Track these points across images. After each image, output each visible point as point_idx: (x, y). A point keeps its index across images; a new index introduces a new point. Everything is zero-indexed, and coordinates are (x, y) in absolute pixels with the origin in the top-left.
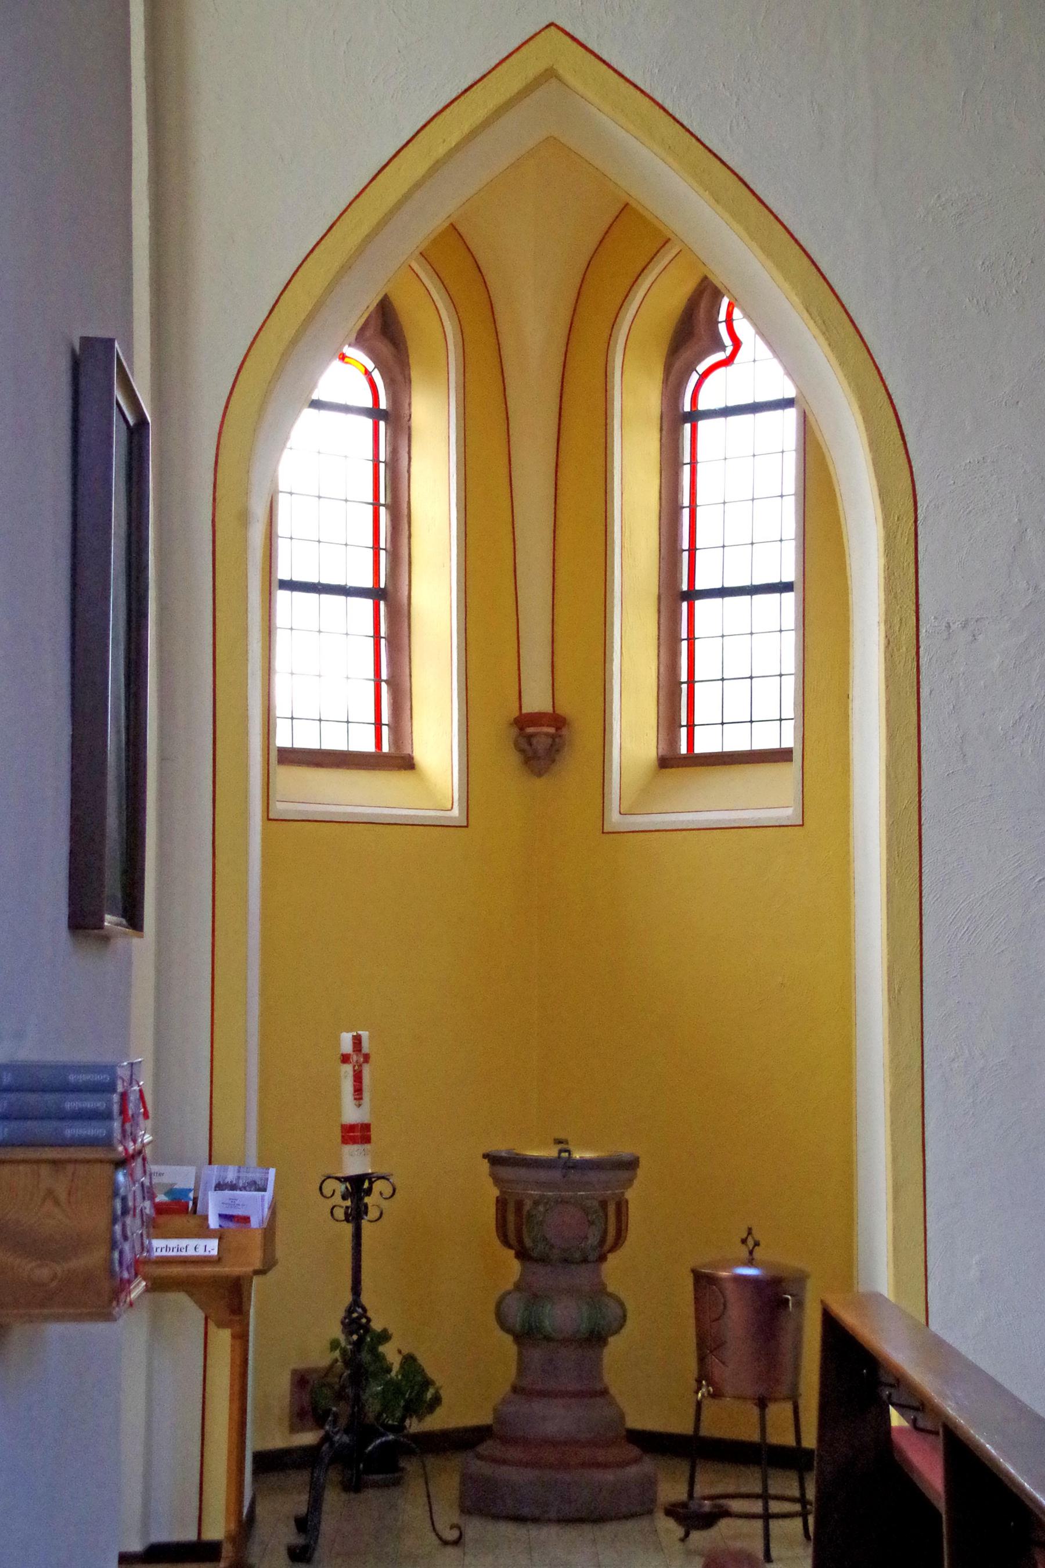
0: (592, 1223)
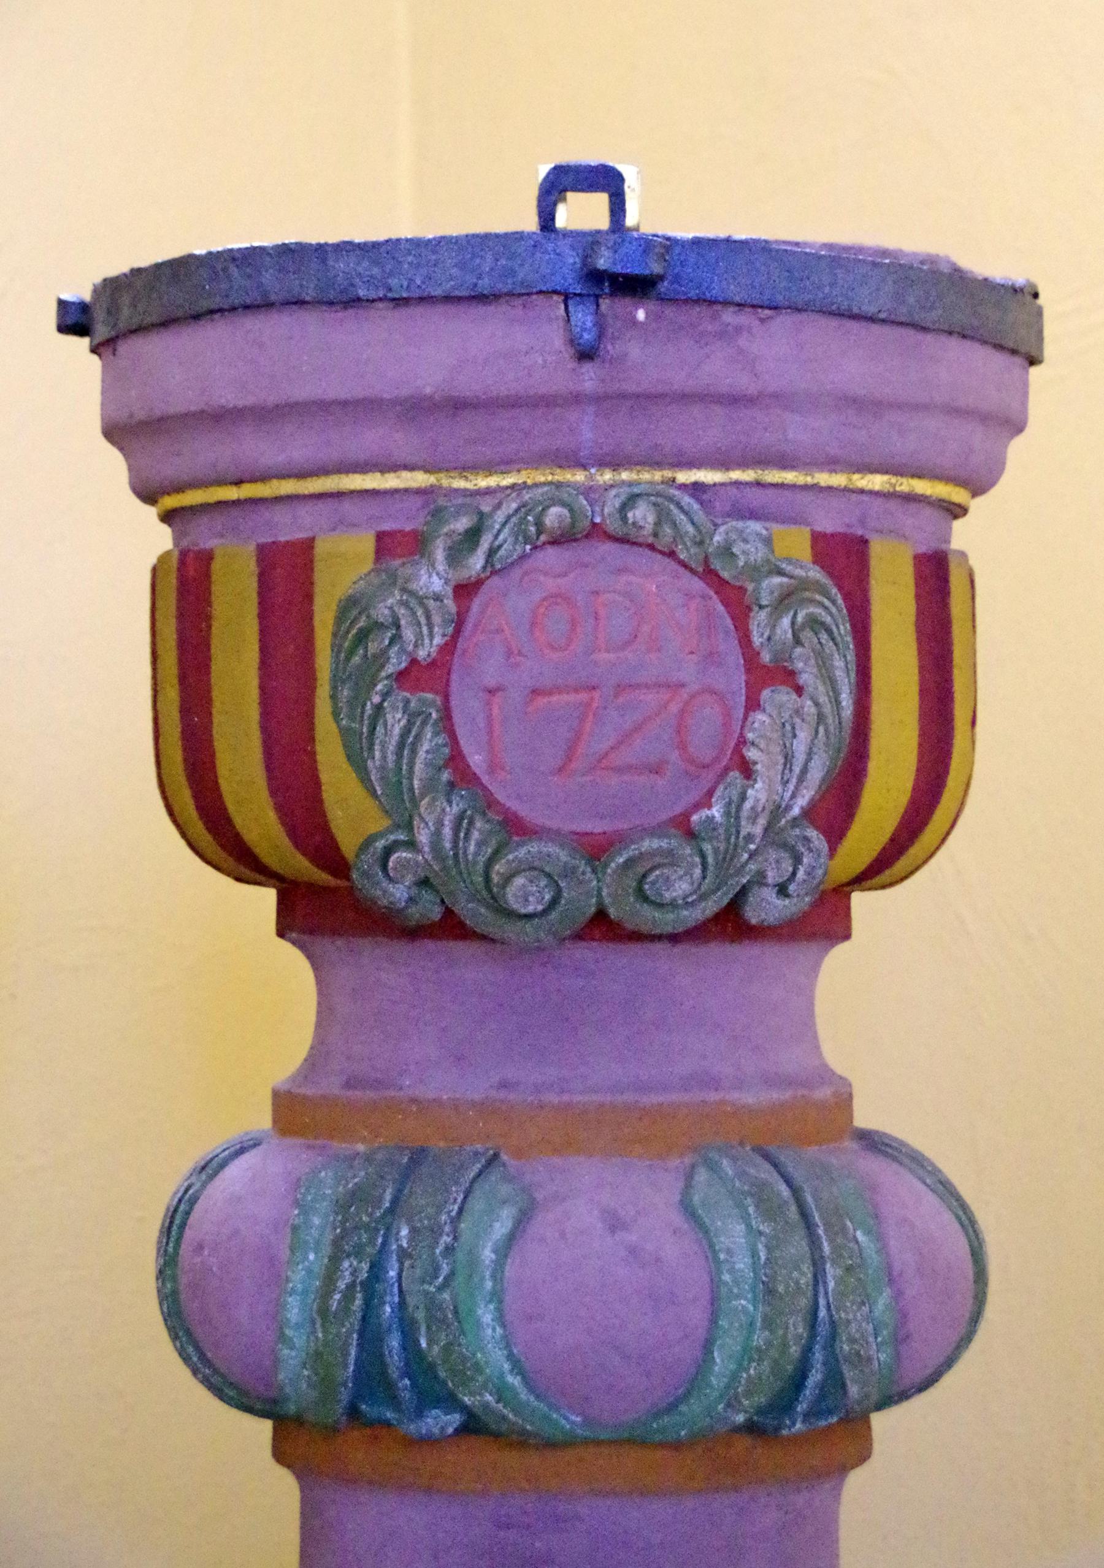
0: (767, 674)
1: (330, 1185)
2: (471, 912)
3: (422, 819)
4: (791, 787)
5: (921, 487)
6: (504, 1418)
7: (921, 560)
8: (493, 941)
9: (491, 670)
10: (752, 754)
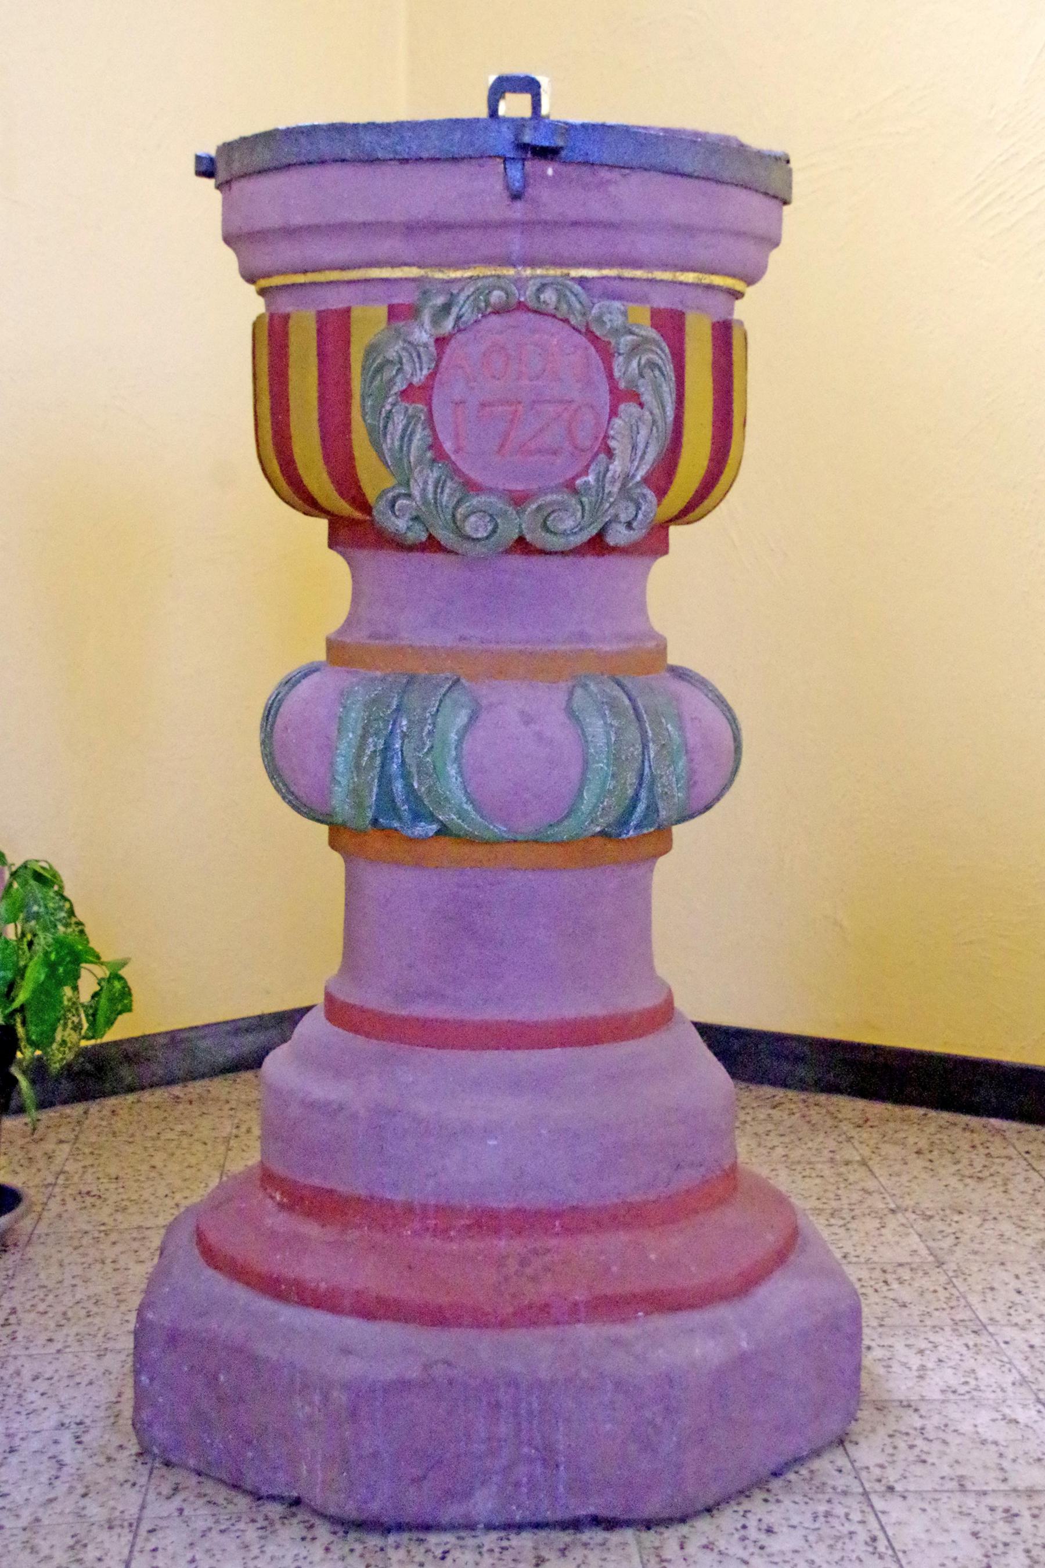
0: (621, 395)
1: (361, 695)
2: (444, 536)
3: (416, 481)
4: (636, 463)
5: (718, 280)
6: (461, 828)
7: (715, 326)
8: (457, 554)
9: (458, 391)
10: (612, 444)
